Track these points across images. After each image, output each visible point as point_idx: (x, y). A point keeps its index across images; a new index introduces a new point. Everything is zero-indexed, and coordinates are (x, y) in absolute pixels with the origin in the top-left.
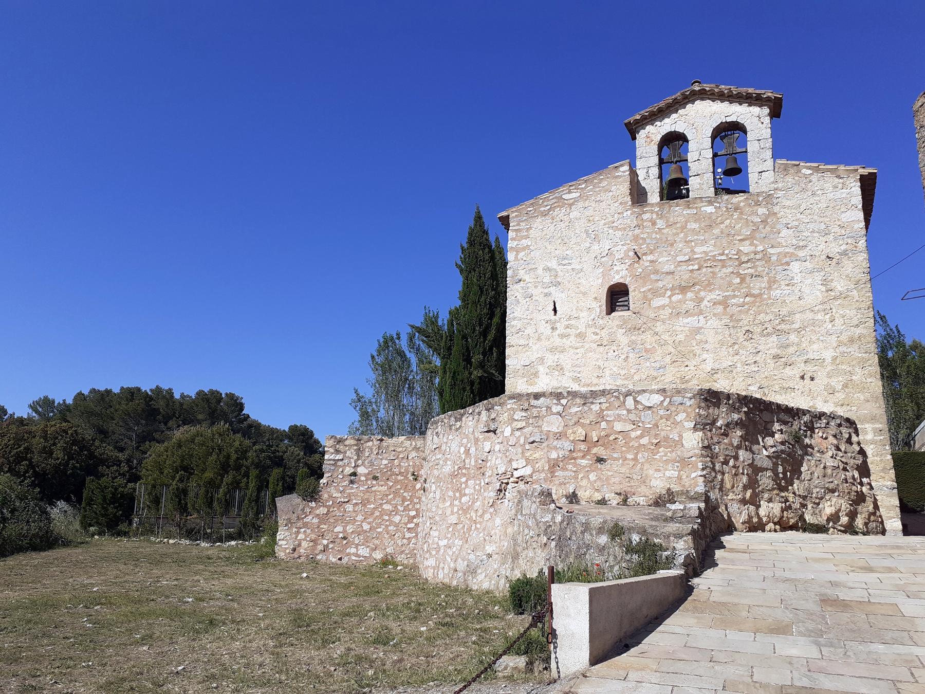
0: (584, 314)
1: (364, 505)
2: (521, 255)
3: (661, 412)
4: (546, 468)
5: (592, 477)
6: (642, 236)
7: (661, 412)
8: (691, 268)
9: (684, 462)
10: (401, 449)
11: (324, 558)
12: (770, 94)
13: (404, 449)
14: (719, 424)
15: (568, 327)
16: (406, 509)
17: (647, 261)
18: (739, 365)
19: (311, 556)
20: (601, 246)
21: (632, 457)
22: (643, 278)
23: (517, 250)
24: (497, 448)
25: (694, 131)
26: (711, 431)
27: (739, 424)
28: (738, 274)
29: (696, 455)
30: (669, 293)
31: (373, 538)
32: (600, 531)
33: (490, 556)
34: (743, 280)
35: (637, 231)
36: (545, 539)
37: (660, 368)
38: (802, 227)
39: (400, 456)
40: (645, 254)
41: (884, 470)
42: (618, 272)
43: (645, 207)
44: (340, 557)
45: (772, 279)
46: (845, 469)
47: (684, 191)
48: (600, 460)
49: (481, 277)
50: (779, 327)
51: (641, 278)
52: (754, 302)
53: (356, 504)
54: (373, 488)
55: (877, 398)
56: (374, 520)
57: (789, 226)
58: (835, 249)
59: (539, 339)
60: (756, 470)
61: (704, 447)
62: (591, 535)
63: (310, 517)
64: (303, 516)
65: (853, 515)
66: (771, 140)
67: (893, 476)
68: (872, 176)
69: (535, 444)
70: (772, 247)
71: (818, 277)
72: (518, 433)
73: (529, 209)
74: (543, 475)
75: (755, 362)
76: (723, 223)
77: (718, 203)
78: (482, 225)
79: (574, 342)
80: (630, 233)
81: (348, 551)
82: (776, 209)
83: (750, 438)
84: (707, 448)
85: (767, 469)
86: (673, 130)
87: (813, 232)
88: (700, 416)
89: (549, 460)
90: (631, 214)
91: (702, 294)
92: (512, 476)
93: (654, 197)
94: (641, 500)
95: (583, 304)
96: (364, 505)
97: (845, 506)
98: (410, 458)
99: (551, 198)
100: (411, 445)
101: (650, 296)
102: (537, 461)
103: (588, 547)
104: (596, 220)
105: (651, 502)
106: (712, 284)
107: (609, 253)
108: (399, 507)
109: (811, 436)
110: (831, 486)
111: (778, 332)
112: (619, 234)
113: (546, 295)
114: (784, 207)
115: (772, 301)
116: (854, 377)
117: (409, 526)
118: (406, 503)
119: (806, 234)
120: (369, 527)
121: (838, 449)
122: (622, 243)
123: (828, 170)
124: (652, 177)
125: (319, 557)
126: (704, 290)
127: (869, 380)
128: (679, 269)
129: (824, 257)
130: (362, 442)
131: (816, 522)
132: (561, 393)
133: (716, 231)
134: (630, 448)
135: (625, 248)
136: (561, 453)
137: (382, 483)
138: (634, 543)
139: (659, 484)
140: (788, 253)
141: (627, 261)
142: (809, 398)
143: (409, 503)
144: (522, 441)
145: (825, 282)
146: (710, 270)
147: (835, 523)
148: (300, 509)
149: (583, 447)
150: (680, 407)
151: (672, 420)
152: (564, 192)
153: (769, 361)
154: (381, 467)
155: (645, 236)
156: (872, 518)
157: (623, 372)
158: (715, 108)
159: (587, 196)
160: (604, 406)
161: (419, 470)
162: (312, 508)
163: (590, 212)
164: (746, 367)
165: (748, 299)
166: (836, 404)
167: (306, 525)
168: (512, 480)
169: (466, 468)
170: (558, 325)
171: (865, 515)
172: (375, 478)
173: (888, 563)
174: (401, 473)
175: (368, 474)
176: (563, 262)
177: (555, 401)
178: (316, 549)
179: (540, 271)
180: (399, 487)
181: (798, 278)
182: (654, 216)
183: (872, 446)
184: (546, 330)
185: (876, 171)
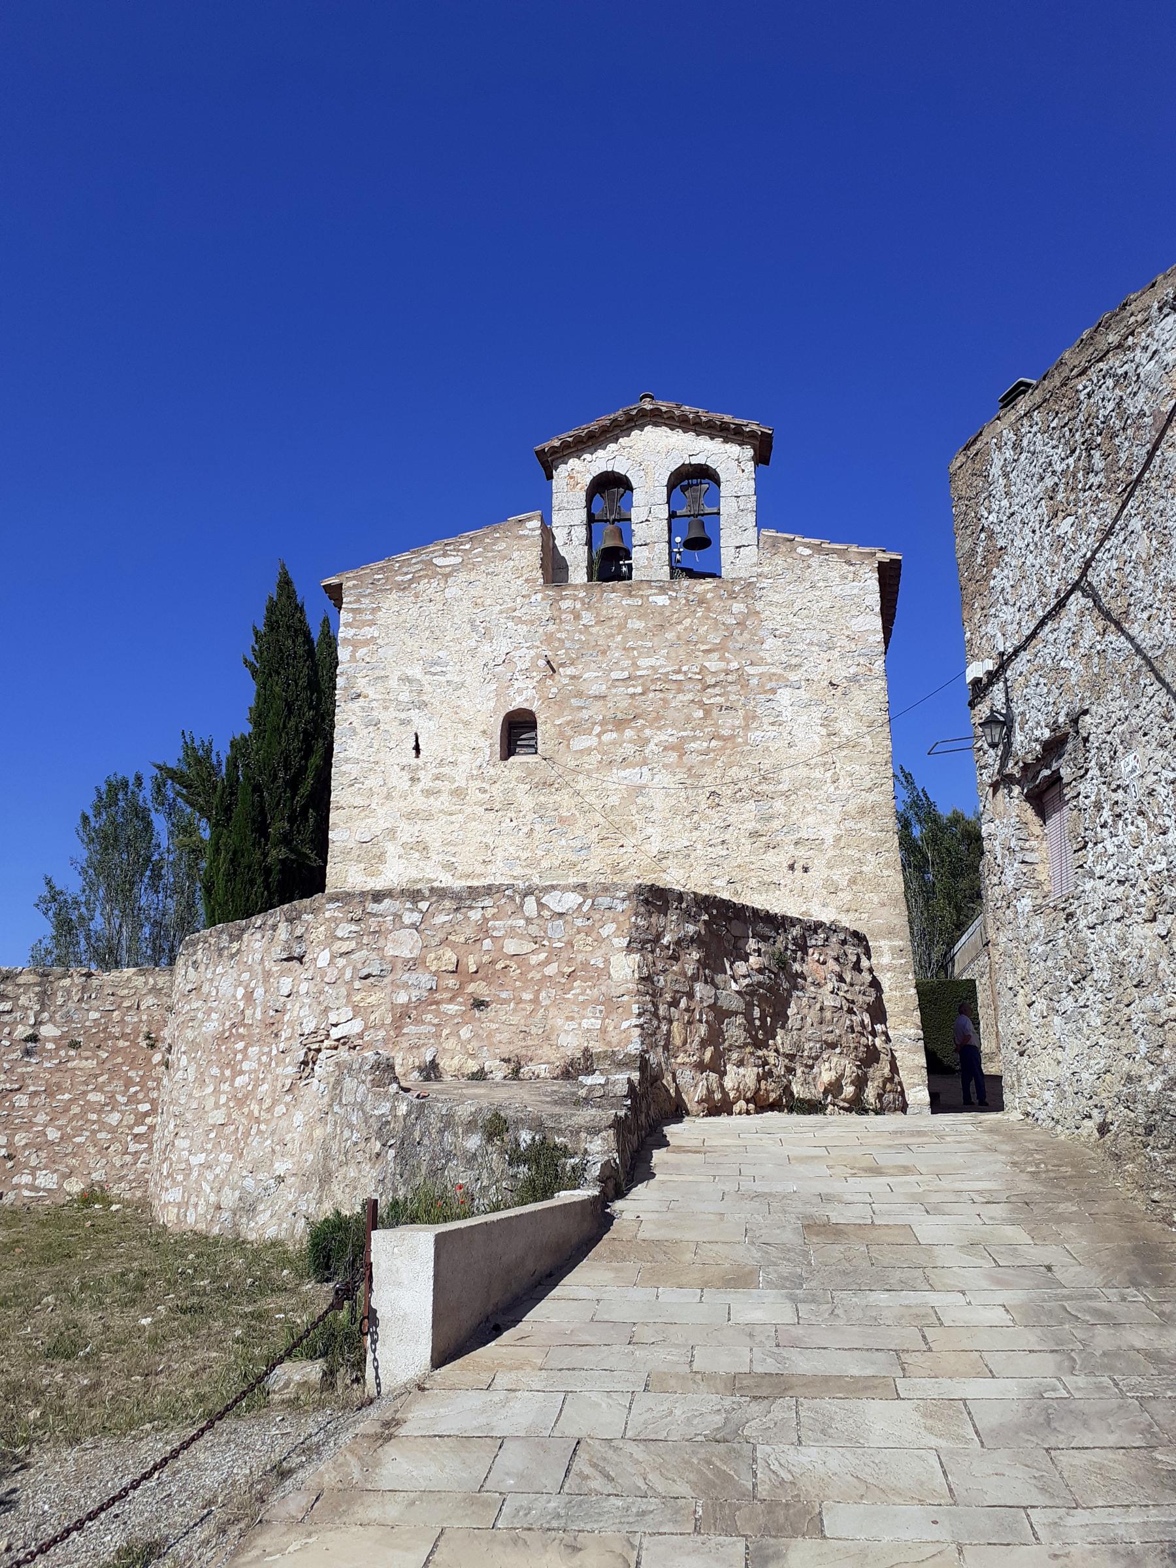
0: (465, 757)
3: (579, 922)
4: (388, 1021)
5: (465, 1033)
6: (559, 635)
7: (579, 922)
8: (631, 690)
9: (610, 1004)
10: (126, 991)
14: (665, 941)
15: (437, 779)
16: (133, 1100)
17: (566, 676)
18: (699, 847)
21: (531, 997)
22: (559, 702)
23: (355, 644)
24: (304, 987)
25: (642, 473)
26: (652, 952)
27: (696, 940)
28: (702, 705)
29: (628, 993)
30: (597, 729)
31: (66, 1155)
34: (707, 713)
35: (551, 627)
36: (378, 1145)
40: (562, 665)
42: (520, 691)
43: (564, 590)
46: (850, 1011)
47: (624, 569)
48: (479, 1004)
50: (758, 789)
52: (723, 748)
53: (35, 1094)
54: (69, 1065)
57: (777, 633)
58: (840, 672)
59: (389, 797)
60: (720, 1014)
62: (456, 1134)
65: (861, 1083)
67: (918, 1021)
69: (371, 980)
71: (817, 713)
72: (341, 962)
74: (382, 1033)
75: (723, 842)
77: (674, 590)
80: (541, 630)
82: (759, 605)
83: (711, 965)
84: (647, 979)
85: (736, 1013)
86: (610, 470)
87: (811, 644)
88: (637, 928)
89: (394, 1006)
90: (543, 599)
91: (648, 732)
92: (328, 1036)
93: (578, 575)
94: (542, 1070)
97: (850, 1069)
98: (142, 1008)
99: (414, 561)
100: (146, 983)
101: (570, 733)
102: (372, 1008)
105: (558, 1071)
109: (803, 959)
110: (831, 1038)
111: (758, 796)
113: (403, 722)
114: (771, 604)
116: (864, 868)
117: (137, 1130)
118: (132, 1090)
120: (59, 1134)
121: (841, 979)
122: (528, 644)
123: (834, 551)
124: (576, 542)
129: (826, 683)
130: (51, 978)
131: (809, 1096)
133: (670, 635)
135: (532, 652)
136: (415, 994)
137: (89, 1054)
139: (570, 1042)
140: (774, 674)
141: (534, 674)
143: (138, 1088)
145: (826, 721)
149: (451, 982)
150: (608, 913)
151: (594, 935)
152: (436, 554)
153: (743, 840)
154: (87, 1024)
155: (563, 635)
157: (524, 855)
160: (489, 913)
164: (710, 849)
165: (714, 743)
166: (840, 909)
168: (327, 1043)
171: (878, 1082)
172: (75, 1045)
175: (61, 1038)
176: (432, 670)
177: (408, 905)
180: (119, 1060)
181: (787, 714)
182: (578, 606)
183: (889, 975)
184: (400, 781)
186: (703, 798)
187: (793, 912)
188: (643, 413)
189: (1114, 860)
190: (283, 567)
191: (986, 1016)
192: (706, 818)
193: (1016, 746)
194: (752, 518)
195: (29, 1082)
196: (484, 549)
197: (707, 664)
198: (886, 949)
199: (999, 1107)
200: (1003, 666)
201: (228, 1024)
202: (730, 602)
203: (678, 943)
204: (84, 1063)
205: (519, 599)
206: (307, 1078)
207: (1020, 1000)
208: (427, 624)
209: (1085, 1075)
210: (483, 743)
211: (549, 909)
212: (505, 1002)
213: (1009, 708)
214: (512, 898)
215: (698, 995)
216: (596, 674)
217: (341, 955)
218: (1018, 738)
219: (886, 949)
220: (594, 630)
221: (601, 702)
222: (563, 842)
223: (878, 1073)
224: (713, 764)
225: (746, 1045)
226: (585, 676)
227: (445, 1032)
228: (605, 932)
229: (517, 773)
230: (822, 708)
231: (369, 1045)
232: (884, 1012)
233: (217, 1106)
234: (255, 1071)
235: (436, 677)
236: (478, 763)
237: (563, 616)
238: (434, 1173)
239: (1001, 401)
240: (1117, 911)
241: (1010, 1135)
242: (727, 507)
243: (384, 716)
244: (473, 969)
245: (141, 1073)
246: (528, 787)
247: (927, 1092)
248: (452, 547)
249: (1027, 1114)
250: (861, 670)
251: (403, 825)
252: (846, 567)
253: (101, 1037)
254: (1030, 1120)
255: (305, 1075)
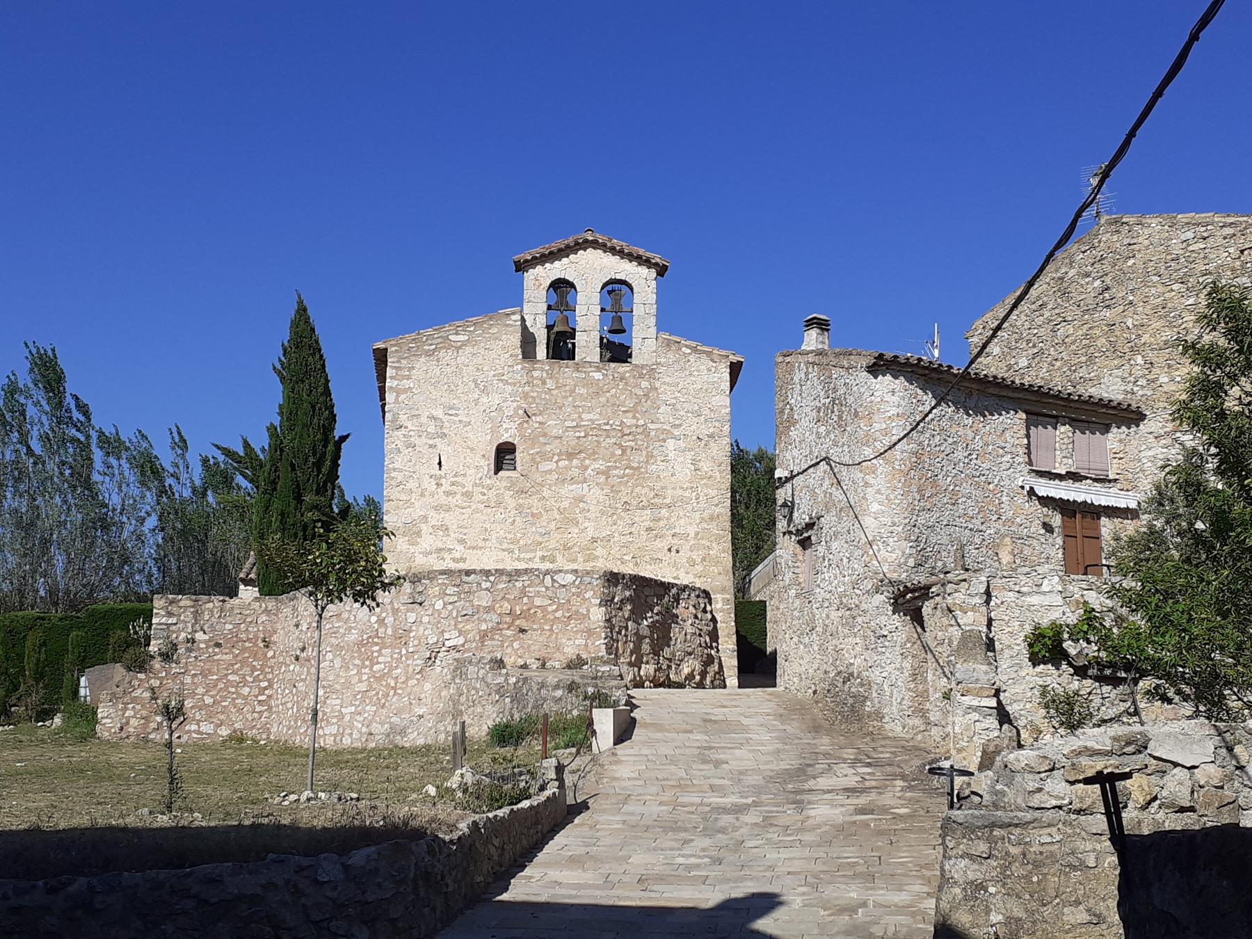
0: (472, 471)
1: (205, 676)
2: (402, 397)
3: (573, 590)
4: (477, 638)
5: (516, 645)
6: (532, 394)
7: (573, 590)
8: (577, 434)
9: (589, 632)
10: (249, 612)
11: (158, 737)
12: (658, 260)
13: (252, 612)
14: (616, 600)
15: (454, 485)
16: (256, 679)
17: (537, 422)
18: (616, 535)
19: (143, 735)
20: (490, 399)
21: (549, 628)
22: (533, 440)
23: (399, 392)
24: (426, 619)
25: (584, 282)
26: (610, 606)
27: (630, 599)
28: (620, 446)
29: (599, 627)
30: (556, 458)
31: (218, 713)
32: (557, 687)
33: (421, 717)
34: (624, 452)
35: (527, 388)
36: (497, 697)
37: (545, 534)
38: (678, 406)
39: (248, 620)
40: (534, 414)
41: (728, 635)
42: (507, 430)
43: (535, 364)
44: (178, 735)
45: (650, 454)
46: (700, 635)
47: (570, 345)
48: (522, 631)
49: (311, 391)
50: (653, 501)
51: (529, 439)
52: (633, 475)
53: (195, 675)
54: (215, 657)
55: (728, 571)
56: (218, 693)
57: (668, 403)
58: (705, 431)
59: (422, 495)
60: (640, 638)
61: (606, 620)
62: (548, 691)
63: (139, 691)
64: (130, 690)
65: (703, 674)
66: (655, 306)
67: (735, 641)
68: (740, 364)
69: (467, 617)
70: (652, 422)
71: (689, 455)
72: (450, 607)
73: (411, 345)
74: (474, 644)
75: (630, 533)
76: (609, 392)
77: (606, 370)
78: (307, 321)
79: (460, 501)
80: (520, 390)
81: (187, 728)
82: (657, 384)
83: (637, 615)
84: (608, 621)
85: (646, 637)
86: (562, 277)
87: (688, 412)
88: (604, 593)
89: (480, 631)
90: (522, 369)
91: (587, 462)
92: (444, 645)
93: (541, 351)
94: (557, 664)
95: (471, 461)
96: (205, 676)
97: (698, 667)
98: (259, 622)
99: (436, 336)
100: (261, 607)
101: (539, 459)
102: (469, 632)
103: (545, 700)
104: (485, 369)
105: (565, 665)
106: (596, 453)
107: (499, 409)
108: (248, 678)
109: (677, 607)
110: (690, 650)
111: (653, 506)
112: (509, 388)
113: (431, 446)
114: (664, 383)
115: (648, 475)
116: (711, 552)
117: (260, 698)
118: (256, 673)
119: (682, 413)
120: (212, 700)
121: (696, 617)
122: (512, 399)
123: (704, 352)
124: (539, 325)
125: (152, 736)
126: (589, 459)
127: (722, 555)
128: (567, 434)
129: (695, 438)
130: (200, 603)
131: (678, 680)
132: (490, 571)
133: (603, 399)
134: (547, 621)
135: (515, 404)
136: (490, 625)
137: (227, 651)
138: (590, 693)
139: (570, 651)
140: (665, 430)
141: (516, 419)
142: (674, 569)
143: (259, 672)
144: (455, 615)
145: (694, 462)
146: (596, 438)
147: (690, 681)
148: (126, 682)
149: (508, 619)
150: (588, 586)
151: (581, 597)
152: (451, 332)
153: (642, 533)
154: (225, 632)
155: (535, 394)
156: (717, 676)
157: (509, 536)
158: (605, 261)
159: (475, 341)
160: (526, 583)
161: (271, 636)
162: (141, 680)
163: (479, 360)
164: (622, 537)
165: (627, 471)
166: (695, 576)
167: (134, 700)
168: (444, 649)
169: (379, 638)
170: (443, 481)
171: (712, 674)
172: (218, 645)
173: (734, 703)
174: (249, 640)
175: (209, 640)
176: (450, 412)
177: (484, 578)
178: (148, 727)
179: (424, 419)
180: (247, 655)
181: (671, 455)
182: (545, 375)
183: (721, 614)
185: (743, 360)
186: (619, 505)
187: (668, 579)
188: (586, 241)
189: (827, 582)
190: (299, 297)
191: (772, 630)
192: (621, 518)
193: (794, 518)
194: (653, 320)
195: (190, 668)
196: (483, 331)
197: (625, 420)
198: (720, 600)
199: (774, 685)
200: (792, 477)
201: (365, 637)
202: (640, 380)
203: (622, 601)
204: (225, 657)
205: (506, 368)
206: (430, 666)
207: (787, 636)
208: (445, 381)
209: (810, 671)
210: (483, 463)
211: (558, 582)
212: (535, 630)
213: (793, 498)
214: (538, 576)
215: (630, 629)
216: (555, 422)
217: (450, 603)
218: (796, 514)
219: (720, 600)
220: (554, 392)
221: (559, 440)
222: (534, 529)
223: (712, 669)
224: (626, 484)
225: (650, 653)
226: (549, 423)
227: (505, 645)
228: (587, 596)
229: (504, 484)
230: (693, 453)
231: (468, 650)
232: (717, 637)
233: (360, 681)
234: (389, 662)
235: (452, 417)
236: (479, 476)
237: (535, 382)
238: (536, 707)
239: (807, 321)
240: (826, 604)
241: (778, 695)
242: (638, 310)
243: (417, 441)
244: (519, 612)
245: (261, 663)
246: (512, 493)
247: (737, 680)
248: (461, 329)
249: (786, 688)
250: (717, 431)
251: (432, 513)
252: (711, 363)
253: (234, 640)
254: (787, 691)
255: (429, 664)
